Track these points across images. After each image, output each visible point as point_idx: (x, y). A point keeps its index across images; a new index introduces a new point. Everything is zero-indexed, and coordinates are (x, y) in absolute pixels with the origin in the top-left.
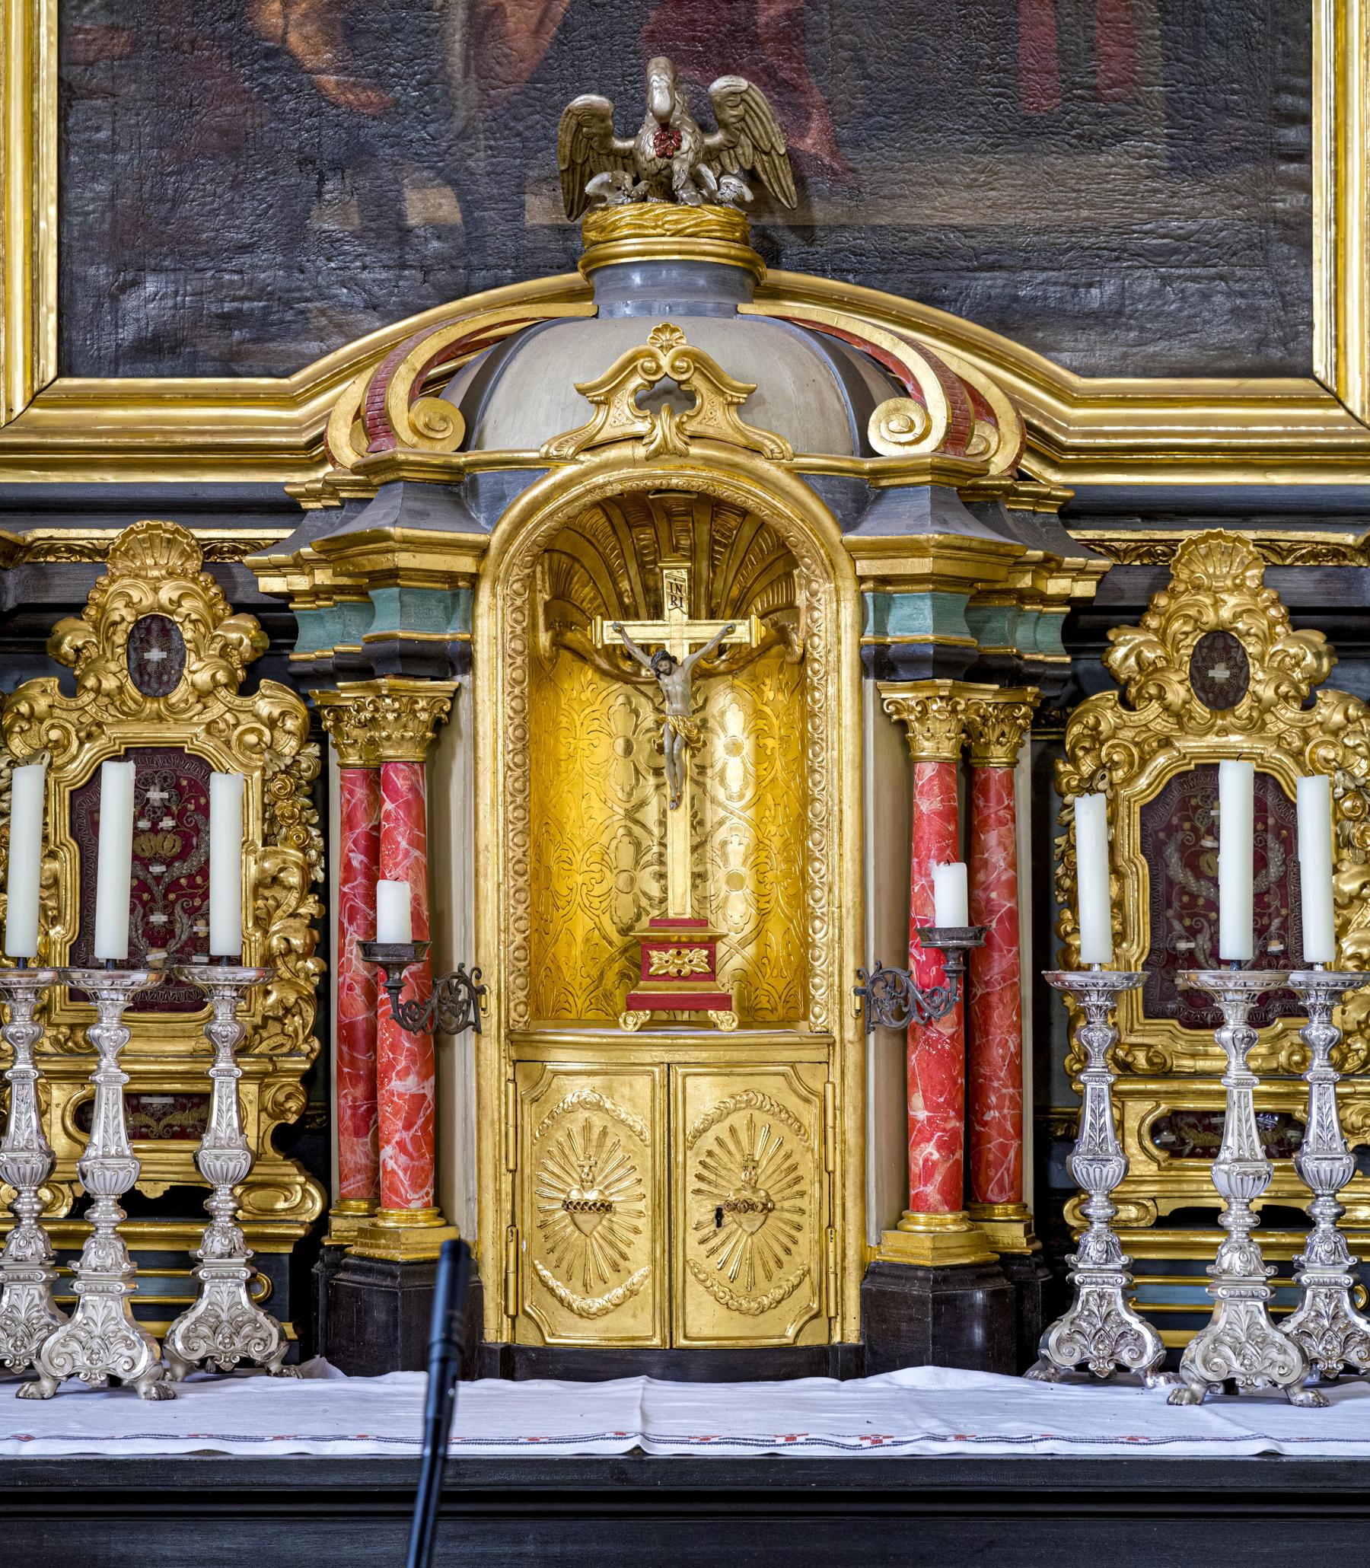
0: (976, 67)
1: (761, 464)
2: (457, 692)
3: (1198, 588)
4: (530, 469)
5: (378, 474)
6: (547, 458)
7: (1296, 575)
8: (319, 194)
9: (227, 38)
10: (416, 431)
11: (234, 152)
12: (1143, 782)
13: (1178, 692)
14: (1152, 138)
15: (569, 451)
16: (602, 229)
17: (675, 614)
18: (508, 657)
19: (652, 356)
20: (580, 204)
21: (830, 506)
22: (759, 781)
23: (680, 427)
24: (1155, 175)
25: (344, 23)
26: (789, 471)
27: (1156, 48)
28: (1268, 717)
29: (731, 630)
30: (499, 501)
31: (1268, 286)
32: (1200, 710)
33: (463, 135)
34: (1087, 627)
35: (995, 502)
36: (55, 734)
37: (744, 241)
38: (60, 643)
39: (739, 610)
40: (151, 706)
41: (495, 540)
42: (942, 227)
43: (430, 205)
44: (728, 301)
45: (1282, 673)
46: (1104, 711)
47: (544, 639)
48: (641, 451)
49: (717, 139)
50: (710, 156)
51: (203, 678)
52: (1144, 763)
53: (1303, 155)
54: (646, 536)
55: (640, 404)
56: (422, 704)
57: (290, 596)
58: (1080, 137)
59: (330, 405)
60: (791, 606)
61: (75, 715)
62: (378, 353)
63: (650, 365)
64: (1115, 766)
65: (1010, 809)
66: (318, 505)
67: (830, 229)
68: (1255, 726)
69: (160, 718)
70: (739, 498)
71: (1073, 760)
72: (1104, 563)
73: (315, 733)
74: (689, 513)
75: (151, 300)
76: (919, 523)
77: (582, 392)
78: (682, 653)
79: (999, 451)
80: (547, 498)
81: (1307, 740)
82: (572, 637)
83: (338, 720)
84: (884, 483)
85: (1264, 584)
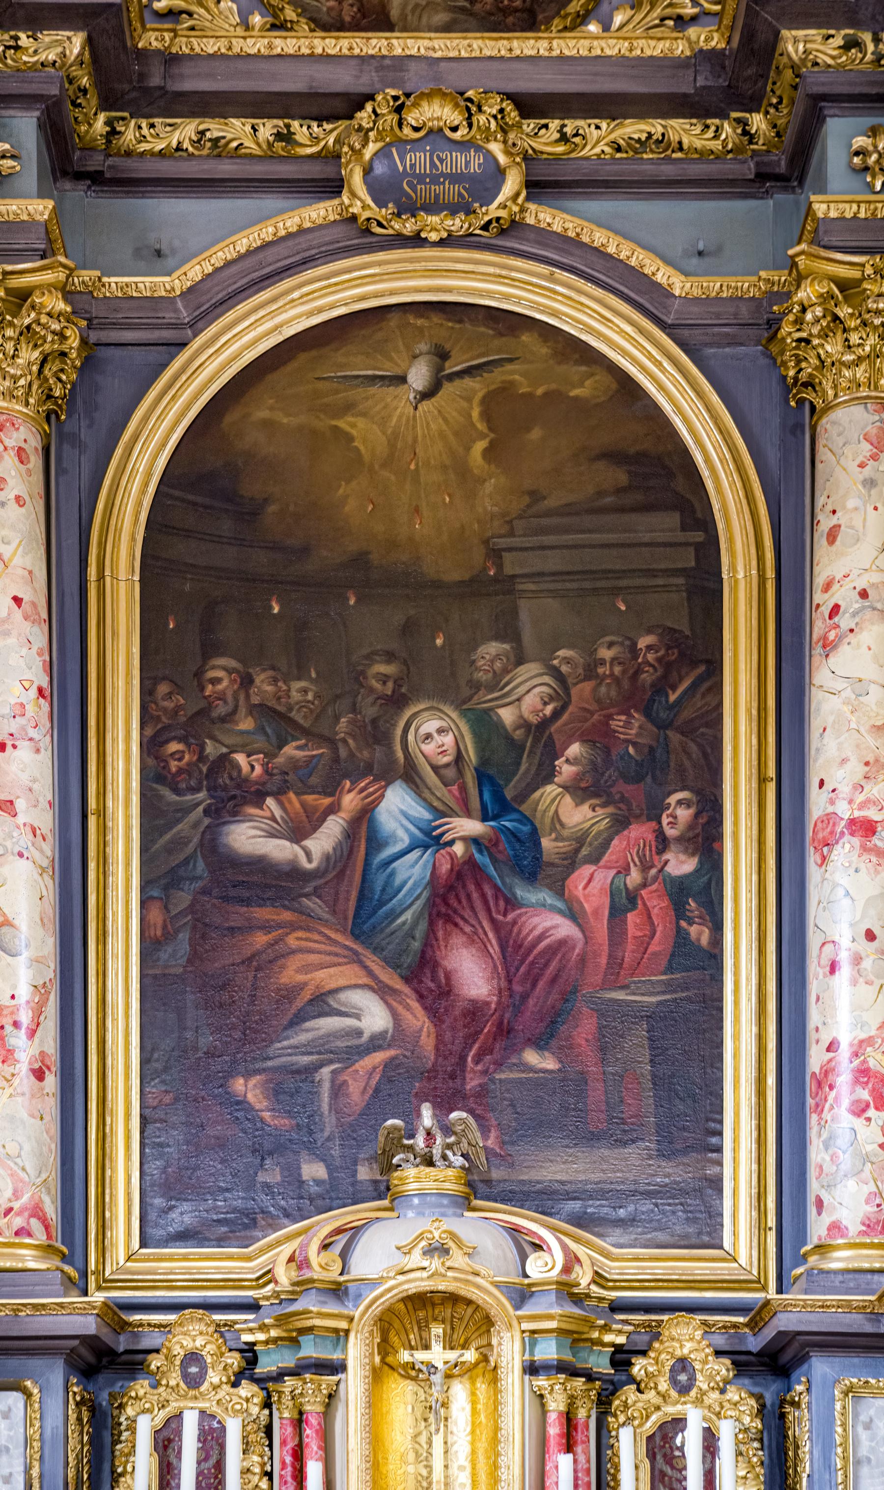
0: (567, 1109)
1: (478, 1280)
2: (339, 1381)
3: (673, 1339)
4: (374, 1283)
5: (302, 1286)
6: (382, 1277)
7: (716, 1337)
8: (262, 1166)
9: (220, 1095)
10: (321, 1266)
11: (222, 1146)
12: (649, 1424)
13: (663, 1386)
14: (650, 1141)
15: (392, 1274)
16: (401, 1179)
17: (437, 1348)
18: (363, 1366)
19: (431, 1232)
20: (389, 1168)
21: (510, 1299)
22: (473, 1423)
23: (443, 1264)
24: (650, 1157)
25: (273, 1089)
26: (492, 1283)
27: (651, 1101)
28: (705, 1397)
29: (462, 1355)
30: (359, 1296)
31: (702, 1209)
32: (674, 1394)
33: (328, 1139)
34: (622, 1358)
35: (581, 1300)
36: (147, 1406)
37: (465, 1184)
38: (149, 1366)
39: (465, 1346)
40: (192, 1393)
41: (357, 1315)
42: (551, 1181)
43: (313, 1171)
44: (459, 1211)
45: (711, 1378)
46: (629, 1393)
47: (377, 1359)
48: (425, 1274)
49: (452, 1139)
50: (449, 1146)
51: (216, 1380)
52: (648, 1417)
53: (719, 1149)
54: (421, 1314)
55: (424, 1253)
56: (324, 1386)
57: (254, 1344)
58: (616, 1141)
59: (273, 1257)
60: (489, 1345)
61: (156, 1397)
62: (305, 1231)
63: (429, 1236)
64: (634, 1418)
65: (587, 1437)
66: (268, 1303)
67: (500, 1181)
68: (699, 1401)
69: (196, 1398)
70: (469, 1295)
71: (615, 1416)
72: (630, 1328)
73: (267, 1404)
74: (442, 1304)
75: (184, 1215)
76: (551, 1306)
77: (398, 1248)
78: (440, 1365)
79: (583, 1278)
80: (382, 1295)
81: (722, 1407)
82: (390, 1359)
83: (280, 1397)
84: (534, 1289)
85: (703, 1338)
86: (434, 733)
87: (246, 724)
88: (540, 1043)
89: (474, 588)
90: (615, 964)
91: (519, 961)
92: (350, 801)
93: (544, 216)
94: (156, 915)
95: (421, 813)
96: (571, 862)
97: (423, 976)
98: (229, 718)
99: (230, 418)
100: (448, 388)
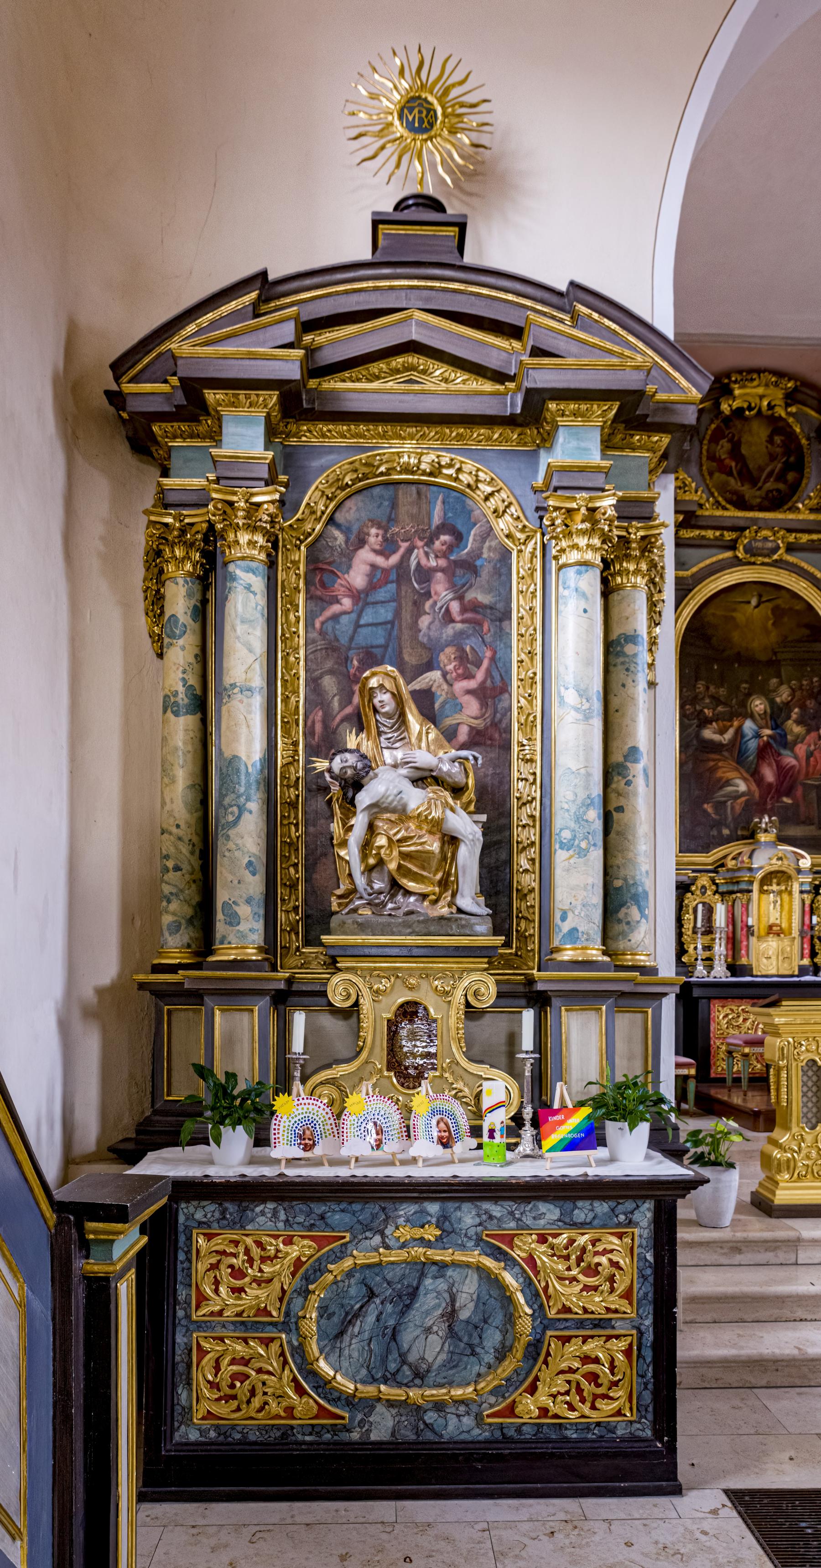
86: (759, 705)
87: (707, 701)
88: (787, 795)
89: (770, 663)
90: (807, 774)
91: (783, 772)
92: (736, 723)
93: (789, 558)
94: (683, 757)
95: (755, 727)
96: (795, 743)
97: (755, 775)
98: (703, 699)
99: (704, 611)
100: (762, 606)
